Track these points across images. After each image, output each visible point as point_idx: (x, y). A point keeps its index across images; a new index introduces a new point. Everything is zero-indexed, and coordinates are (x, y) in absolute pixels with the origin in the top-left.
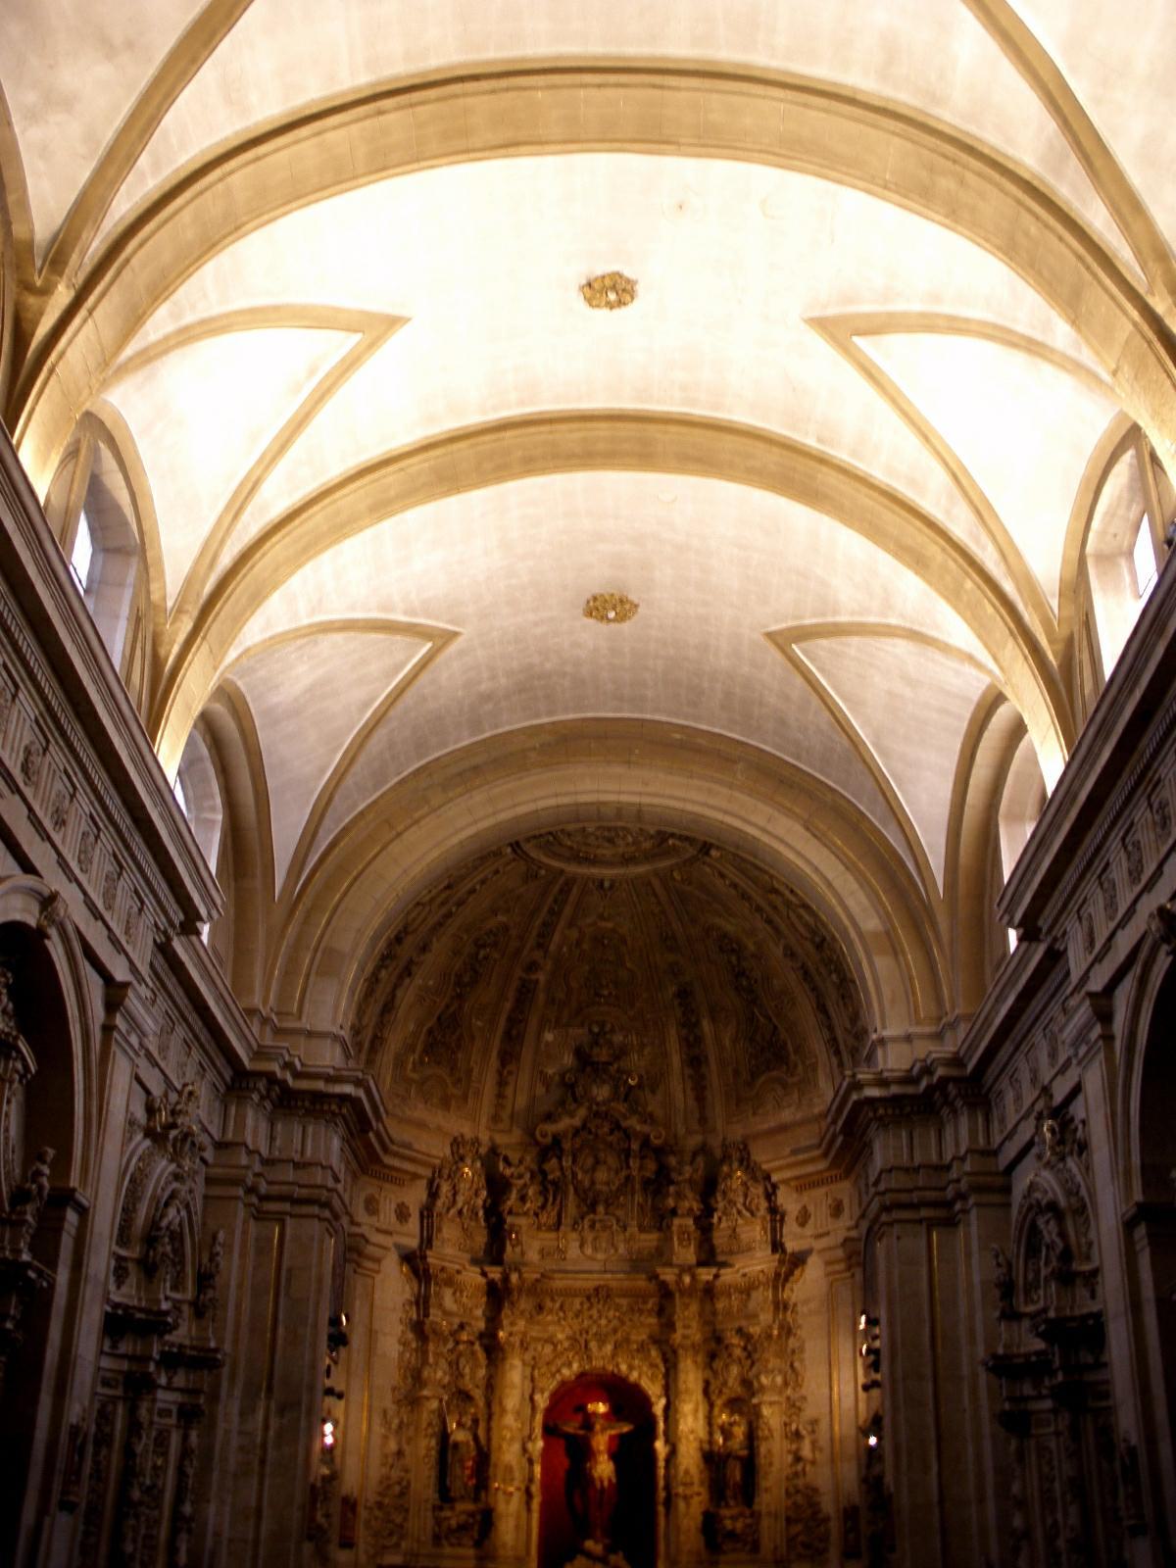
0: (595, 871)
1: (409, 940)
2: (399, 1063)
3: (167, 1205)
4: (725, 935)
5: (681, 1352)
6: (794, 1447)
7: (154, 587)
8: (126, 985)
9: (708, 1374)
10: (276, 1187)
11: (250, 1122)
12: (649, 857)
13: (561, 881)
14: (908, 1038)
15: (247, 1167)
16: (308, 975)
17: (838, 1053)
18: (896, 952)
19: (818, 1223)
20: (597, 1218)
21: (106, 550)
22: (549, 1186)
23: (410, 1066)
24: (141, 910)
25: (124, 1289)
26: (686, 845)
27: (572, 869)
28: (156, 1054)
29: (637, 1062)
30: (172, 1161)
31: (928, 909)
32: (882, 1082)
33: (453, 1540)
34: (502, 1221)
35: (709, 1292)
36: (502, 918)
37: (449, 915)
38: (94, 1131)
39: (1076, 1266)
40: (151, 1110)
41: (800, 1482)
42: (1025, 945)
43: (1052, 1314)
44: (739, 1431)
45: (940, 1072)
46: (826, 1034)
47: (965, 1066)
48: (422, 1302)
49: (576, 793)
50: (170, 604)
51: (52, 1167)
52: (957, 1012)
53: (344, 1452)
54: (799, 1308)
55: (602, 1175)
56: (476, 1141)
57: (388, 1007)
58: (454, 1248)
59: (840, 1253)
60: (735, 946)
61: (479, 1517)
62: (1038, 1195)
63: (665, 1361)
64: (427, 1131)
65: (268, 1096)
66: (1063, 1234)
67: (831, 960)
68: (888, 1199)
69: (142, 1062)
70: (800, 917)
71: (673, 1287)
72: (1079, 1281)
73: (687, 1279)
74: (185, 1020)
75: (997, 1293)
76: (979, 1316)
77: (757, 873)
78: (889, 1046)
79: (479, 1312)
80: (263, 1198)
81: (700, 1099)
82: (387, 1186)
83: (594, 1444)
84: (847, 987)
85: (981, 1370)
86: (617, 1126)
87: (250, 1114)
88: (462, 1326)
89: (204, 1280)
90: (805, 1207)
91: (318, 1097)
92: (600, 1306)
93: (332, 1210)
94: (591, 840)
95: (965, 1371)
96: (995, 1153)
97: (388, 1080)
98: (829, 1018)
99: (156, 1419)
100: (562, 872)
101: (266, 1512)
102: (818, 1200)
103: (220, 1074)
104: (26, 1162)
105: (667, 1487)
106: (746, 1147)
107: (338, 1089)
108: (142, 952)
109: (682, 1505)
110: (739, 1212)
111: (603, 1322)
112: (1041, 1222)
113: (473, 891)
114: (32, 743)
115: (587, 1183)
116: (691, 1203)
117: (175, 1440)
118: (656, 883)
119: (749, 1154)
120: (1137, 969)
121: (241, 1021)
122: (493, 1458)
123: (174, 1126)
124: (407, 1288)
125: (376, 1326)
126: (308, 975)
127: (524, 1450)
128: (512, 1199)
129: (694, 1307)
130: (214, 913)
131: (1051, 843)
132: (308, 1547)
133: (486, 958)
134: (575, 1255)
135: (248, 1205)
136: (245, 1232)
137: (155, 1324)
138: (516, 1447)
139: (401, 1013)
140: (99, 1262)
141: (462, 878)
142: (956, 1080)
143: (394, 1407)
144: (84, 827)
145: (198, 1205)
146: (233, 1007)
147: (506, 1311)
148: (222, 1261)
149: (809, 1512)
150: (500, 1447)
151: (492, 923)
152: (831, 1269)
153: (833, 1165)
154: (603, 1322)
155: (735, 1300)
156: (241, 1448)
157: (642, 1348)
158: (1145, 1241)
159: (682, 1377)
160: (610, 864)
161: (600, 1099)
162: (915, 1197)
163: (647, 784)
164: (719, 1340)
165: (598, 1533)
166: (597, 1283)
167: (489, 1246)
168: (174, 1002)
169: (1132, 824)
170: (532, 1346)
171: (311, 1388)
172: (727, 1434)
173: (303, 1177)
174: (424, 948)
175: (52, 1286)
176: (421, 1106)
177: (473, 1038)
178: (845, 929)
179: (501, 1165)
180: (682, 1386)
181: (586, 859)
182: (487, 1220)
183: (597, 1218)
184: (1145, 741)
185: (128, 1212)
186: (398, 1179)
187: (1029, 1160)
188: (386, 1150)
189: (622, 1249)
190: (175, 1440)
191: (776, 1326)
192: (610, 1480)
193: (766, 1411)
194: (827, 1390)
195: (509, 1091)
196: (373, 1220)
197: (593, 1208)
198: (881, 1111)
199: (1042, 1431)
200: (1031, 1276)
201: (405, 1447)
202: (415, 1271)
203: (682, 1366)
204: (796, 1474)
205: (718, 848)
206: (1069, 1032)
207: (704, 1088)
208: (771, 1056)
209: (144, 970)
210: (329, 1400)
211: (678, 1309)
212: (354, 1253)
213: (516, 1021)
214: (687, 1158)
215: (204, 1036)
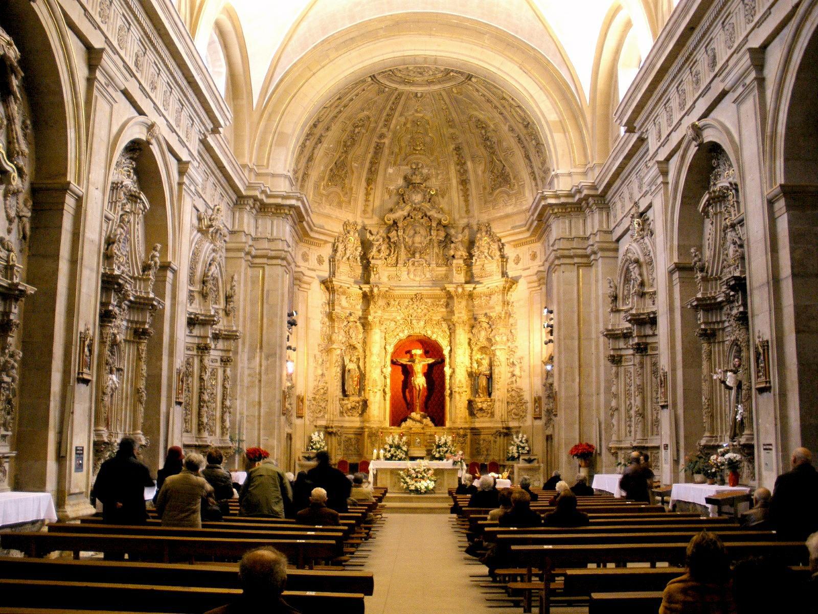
0: (413, 89)
1: (320, 126)
2: (317, 187)
3: (210, 264)
5: (457, 324)
6: (511, 369)
8: (188, 163)
9: (471, 336)
10: (259, 251)
11: (246, 220)
13: (396, 94)
14: (570, 174)
15: (245, 243)
17: (535, 179)
18: (564, 131)
19: (526, 262)
23: (322, 187)
24: (192, 125)
25: (193, 305)
27: (402, 88)
28: (200, 191)
30: (211, 243)
31: (581, 110)
32: (557, 197)
33: (350, 414)
34: (369, 262)
35: (471, 296)
36: (366, 113)
37: (340, 112)
38: (177, 235)
39: (646, 290)
40: (200, 219)
41: (514, 386)
42: (627, 134)
43: (634, 312)
44: (485, 363)
45: (585, 192)
46: (530, 170)
47: (597, 189)
48: (331, 303)
49: (404, 51)
51: (160, 252)
52: (594, 162)
53: (296, 375)
54: (515, 304)
55: (418, 239)
56: (355, 224)
57: (310, 159)
59: (535, 278)
61: (361, 403)
62: (629, 255)
63: (450, 329)
64: (333, 219)
65: (254, 207)
66: (641, 275)
67: (532, 134)
68: (559, 253)
69: (196, 198)
70: (516, 112)
71: (453, 293)
72: (647, 296)
73: (460, 290)
74: (213, 173)
75: (610, 300)
76: (601, 310)
77: (495, 90)
79: (359, 307)
80: (254, 257)
81: (466, 201)
82: (312, 247)
84: (539, 147)
85: (601, 335)
87: (246, 216)
88: (351, 314)
89: (228, 298)
91: (278, 206)
92: (418, 303)
94: (411, 73)
95: (594, 336)
96: (611, 232)
98: (531, 162)
100: (396, 89)
101: (263, 403)
102: (524, 252)
103: (230, 197)
104: (147, 251)
105: (450, 388)
108: (194, 146)
109: (457, 396)
111: (419, 310)
112: (631, 268)
113: (352, 100)
114: (138, 51)
115: (410, 243)
118: (444, 94)
120: (680, 152)
121: (240, 173)
122: (367, 377)
123: (211, 226)
125: (310, 315)
127: (382, 372)
128: (374, 252)
129: (464, 303)
130: (228, 123)
131: (642, 86)
132: (283, 418)
133: (358, 133)
134: (403, 278)
136: (246, 274)
137: (207, 322)
138: (378, 371)
139: (317, 161)
140: (183, 295)
141: (346, 94)
142: (593, 196)
143: (320, 353)
144: (165, 89)
145: (223, 263)
146: (236, 165)
147: (372, 306)
148: (236, 288)
149: (518, 399)
150: (370, 371)
151: (362, 115)
153: (532, 235)
154: (419, 310)
156: (249, 375)
157: (438, 323)
158: (784, 209)
159: (458, 337)
160: (421, 85)
162: (572, 253)
164: (475, 319)
166: (415, 292)
167: (363, 277)
168: (208, 165)
169: (682, 81)
171: (281, 346)
172: (479, 363)
173: (273, 246)
174: (328, 129)
175: (164, 308)
177: (353, 172)
178: (539, 120)
179: (368, 235)
180: (458, 341)
182: (362, 262)
184: (690, 41)
185: (192, 269)
186: (318, 243)
187: (627, 237)
188: (312, 230)
191: (503, 313)
193: (498, 353)
194: (527, 344)
195: (371, 198)
196: (306, 264)
197: (413, 255)
198: (556, 211)
199: (627, 364)
200: (626, 292)
201: (325, 372)
202: (327, 289)
203: (457, 331)
205: (476, 77)
206: (647, 179)
207: (468, 195)
208: (502, 179)
209: (195, 154)
210: (289, 351)
212: (297, 280)
214: (460, 230)
215: (223, 180)
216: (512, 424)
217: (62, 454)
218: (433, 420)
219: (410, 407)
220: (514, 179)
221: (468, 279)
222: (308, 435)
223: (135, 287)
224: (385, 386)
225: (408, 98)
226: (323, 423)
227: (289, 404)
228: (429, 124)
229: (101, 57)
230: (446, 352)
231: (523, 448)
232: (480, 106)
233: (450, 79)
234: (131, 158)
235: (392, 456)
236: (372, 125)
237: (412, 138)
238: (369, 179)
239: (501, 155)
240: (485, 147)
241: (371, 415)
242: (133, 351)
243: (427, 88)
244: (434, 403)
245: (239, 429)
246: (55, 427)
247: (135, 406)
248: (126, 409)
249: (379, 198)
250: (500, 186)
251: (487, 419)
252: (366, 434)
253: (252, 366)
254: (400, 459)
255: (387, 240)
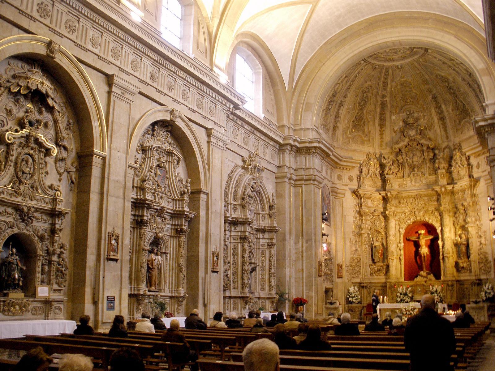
0: (394, 63)
2: (344, 133)
4: (442, 77)
5: (444, 212)
6: (480, 240)
7: (203, 12)
9: (454, 219)
10: (298, 177)
12: (410, 56)
13: (385, 68)
16: (302, 112)
20: (415, 173)
21: (185, 6)
22: (400, 164)
23: (348, 133)
24: (216, 106)
25: (236, 213)
26: (420, 50)
27: (387, 64)
29: (423, 122)
30: (251, 175)
32: (485, 120)
33: (377, 274)
35: (452, 193)
36: (369, 83)
37: (351, 85)
40: (244, 161)
48: (360, 205)
50: (209, 16)
51: (190, 183)
55: (415, 159)
58: (370, 187)
60: (446, 80)
61: (385, 267)
63: (440, 216)
65: (292, 150)
71: (439, 192)
73: (443, 189)
78: (489, 107)
79: (381, 206)
81: (446, 131)
82: (344, 171)
83: (420, 243)
86: (418, 143)
88: (375, 211)
90: (478, 163)
91: (308, 148)
93: (317, 181)
94: (389, 54)
97: (341, 138)
98: (479, 99)
99: (260, 247)
105: (443, 254)
106: (460, 145)
107: (313, 145)
110: (459, 166)
111: (420, 205)
113: (356, 77)
115: (411, 162)
116: (444, 165)
117: (267, 252)
119: (461, 147)
123: (250, 165)
124: (355, 201)
125: (345, 213)
126: (302, 112)
133: (367, 96)
135: (290, 183)
136: (290, 191)
143: (354, 237)
144: (182, 88)
147: (388, 205)
152: (487, 182)
154: (420, 205)
155: (460, 195)
156: (296, 253)
157: (432, 212)
159: (445, 220)
160: (399, 60)
161: (412, 135)
163: (400, 33)
164: (456, 208)
165: (424, 269)
166: (416, 193)
170: (398, 215)
174: (345, 97)
176: (354, 145)
180: (445, 223)
181: (390, 60)
183: (415, 173)
185: (236, 192)
188: (341, 160)
189: (424, 182)
190: (267, 252)
192: (426, 253)
193: (470, 229)
195: (384, 136)
197: (413, 170)
198: (486, 130)
202: (357, 196)
203: (444, 217)
204: (481, 249)
205: (430, 49)
207: (446, 127)
211: (442, 199)
213: (382, 114)
216: (482, 277)
217: (96, 300)
218: (435, 276)
219: (421, 268)
220: (471, 112)
221: (450, 182)
222: (345, 287)
223: (176, 205)
224: (400, 255)
225: (393, 71)
226: (358, 280)
227: (328, 268)
228: (411, 84)
229: (113, 79)
230: (439, 231)
231: (490, 293)
232: (440, 67)
233: (416, 53)
234: (167, 131)
235: (401, 300)
236: (375, 91)
237: (403, 95)
238: (381, 124)
239: (461, 98)
240: (450, 93)
241: (391, 274)
242: (176, 241)
243: (403, 62)
244: (434, 264)
245: (289, 286)
246: (91, 285)
247: (178, 274)
248: (172, 275)
249: (388, 135)
250: (464, 119)
251: (467, 274)
252: (388, 286)
253: (298, 247)
254: (407, 302)
255: (397, 162)
